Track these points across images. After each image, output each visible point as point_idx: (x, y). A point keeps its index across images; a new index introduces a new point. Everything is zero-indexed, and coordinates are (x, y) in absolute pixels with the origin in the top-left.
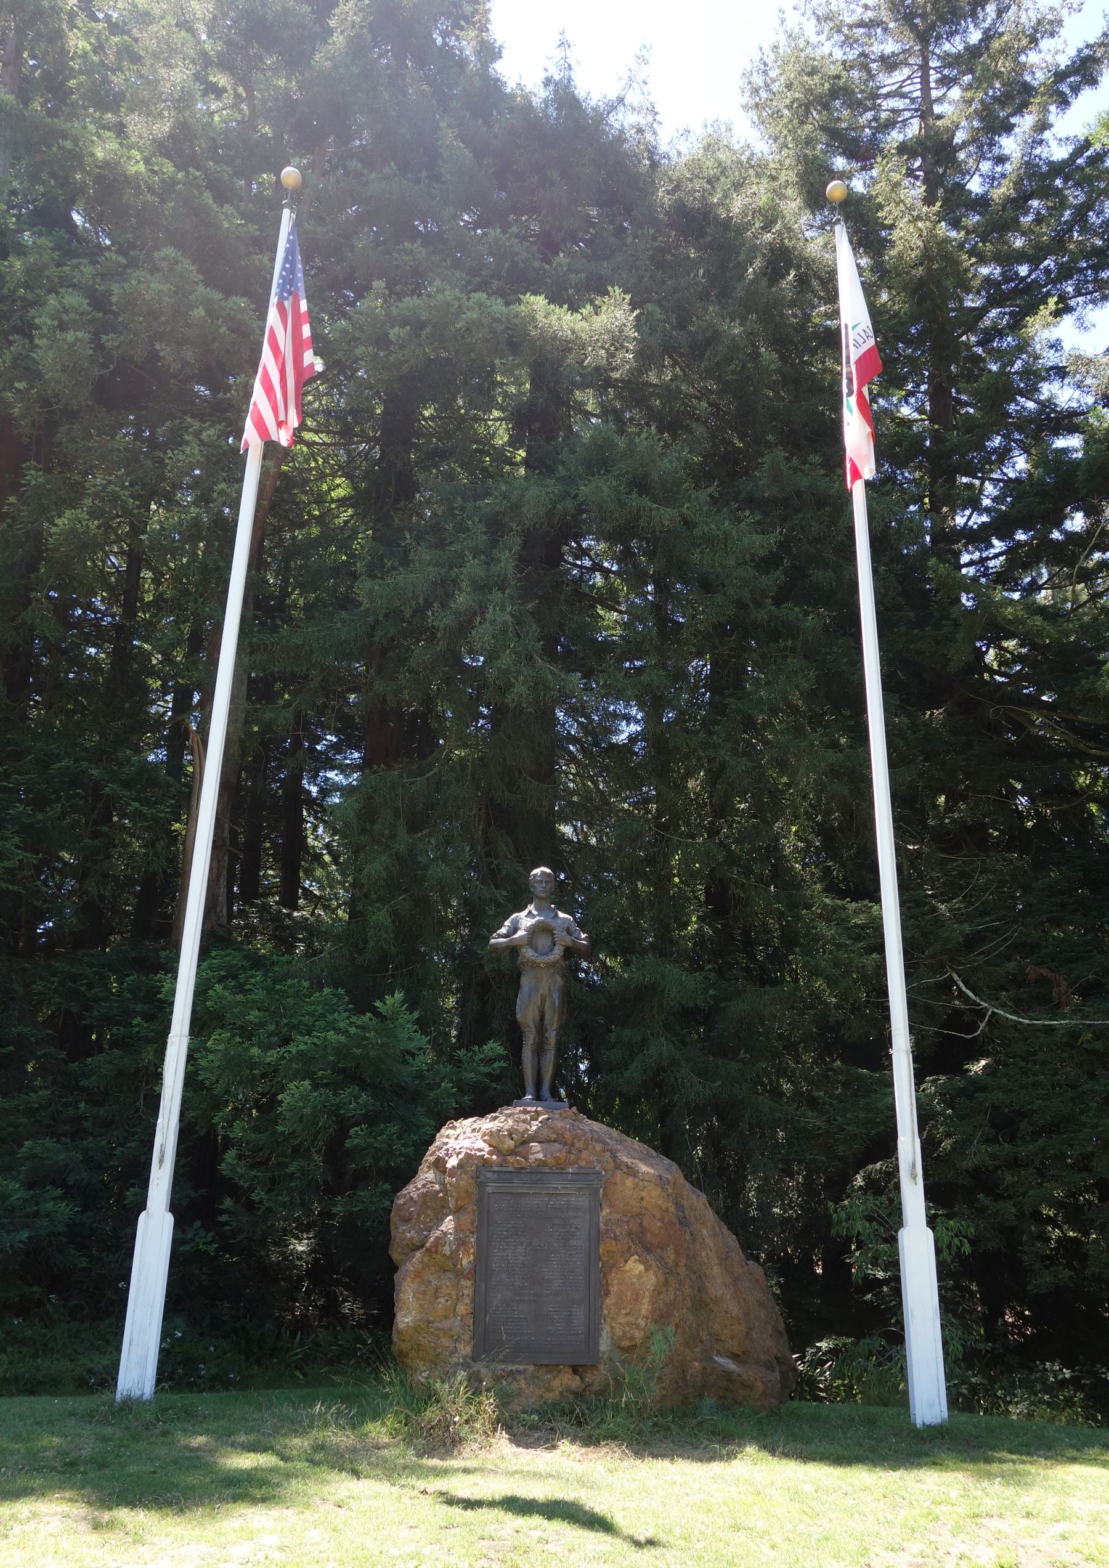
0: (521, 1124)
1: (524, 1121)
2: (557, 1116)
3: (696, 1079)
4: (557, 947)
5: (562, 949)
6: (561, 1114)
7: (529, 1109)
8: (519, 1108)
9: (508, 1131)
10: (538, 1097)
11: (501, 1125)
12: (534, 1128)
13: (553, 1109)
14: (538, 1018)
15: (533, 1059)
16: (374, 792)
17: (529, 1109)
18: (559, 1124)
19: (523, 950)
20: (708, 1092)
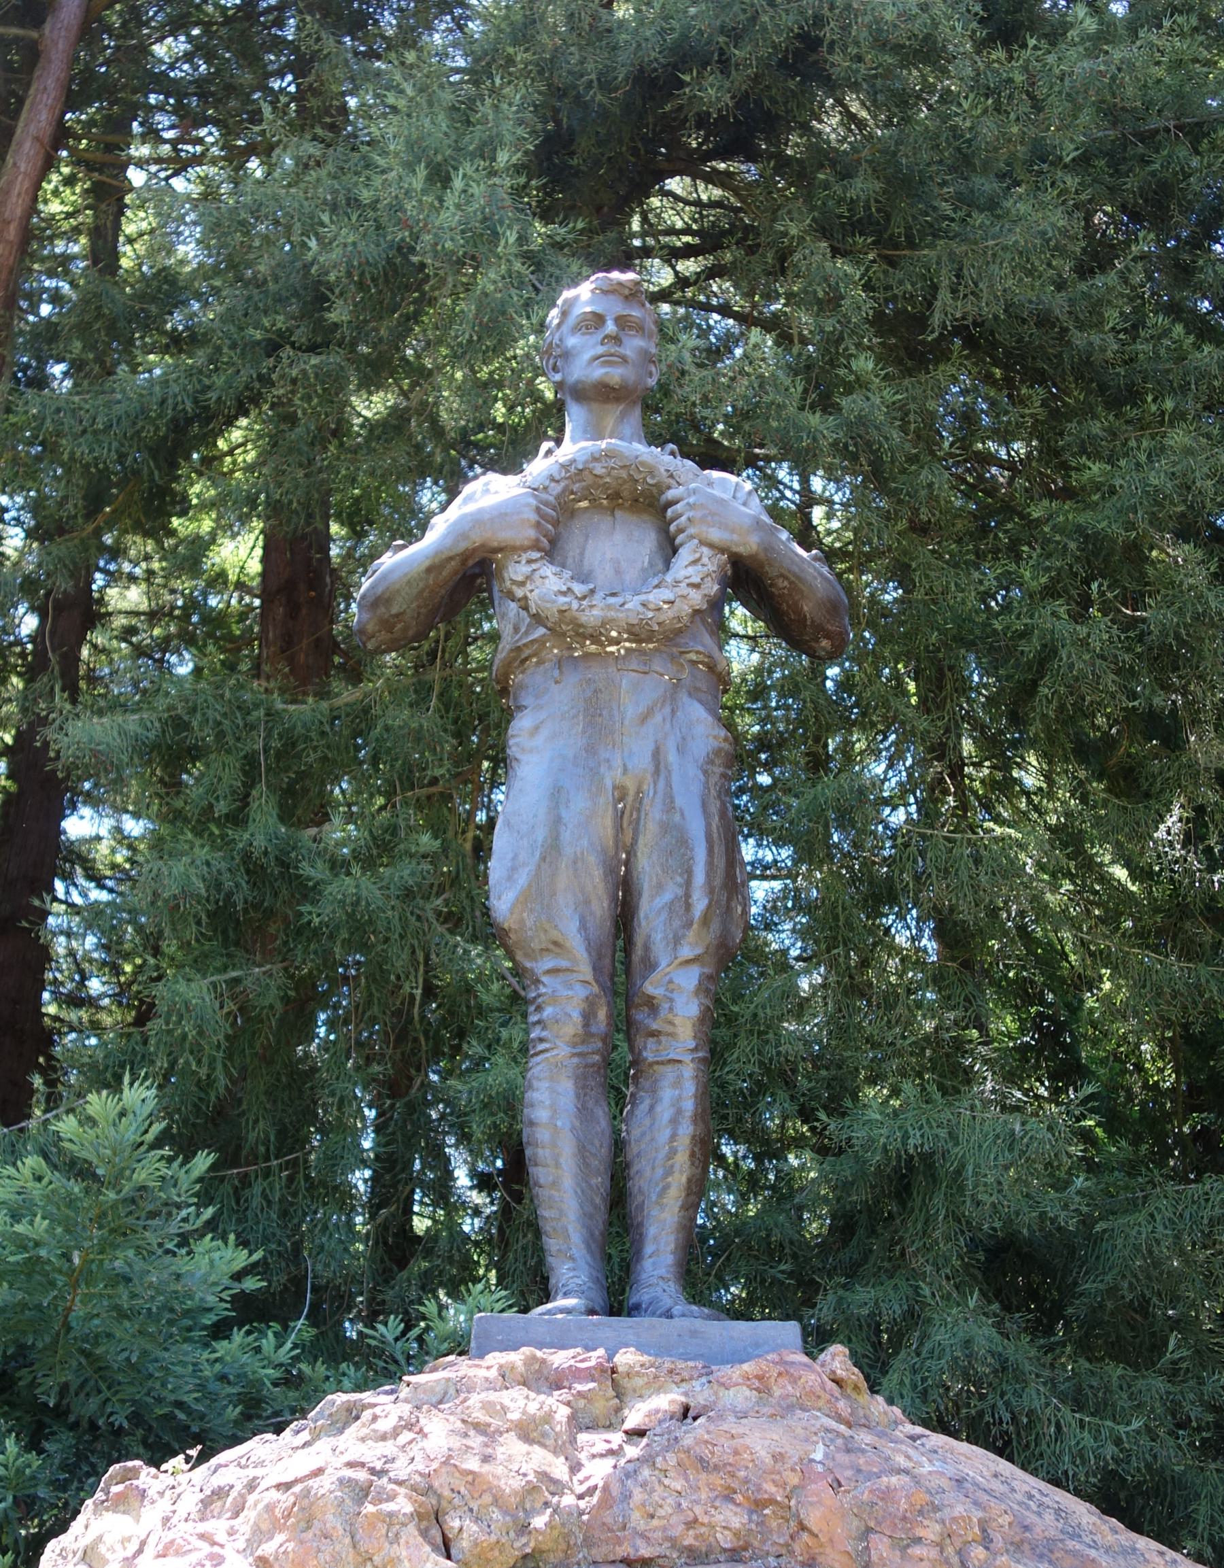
0: (512, 1446)
1: (529, 1431)
2: (740, 1396)
3: (1068, 1415)
4: (685, 555)
5: (712, 563)
6: (762, 1385)
7: (560, 1359)
8: (496, 1358)
9: (424, 1489)
10: (616, 1297)
11: (372, 1453)
12: (598, 1471)
13: (711, 1361)
14: (601, 907)
15: (583, 1111)
16: (193, 711)
17: (560, 1359)
18: (761, 1441)
19: (516, 570)
20: (1110, 1450)
